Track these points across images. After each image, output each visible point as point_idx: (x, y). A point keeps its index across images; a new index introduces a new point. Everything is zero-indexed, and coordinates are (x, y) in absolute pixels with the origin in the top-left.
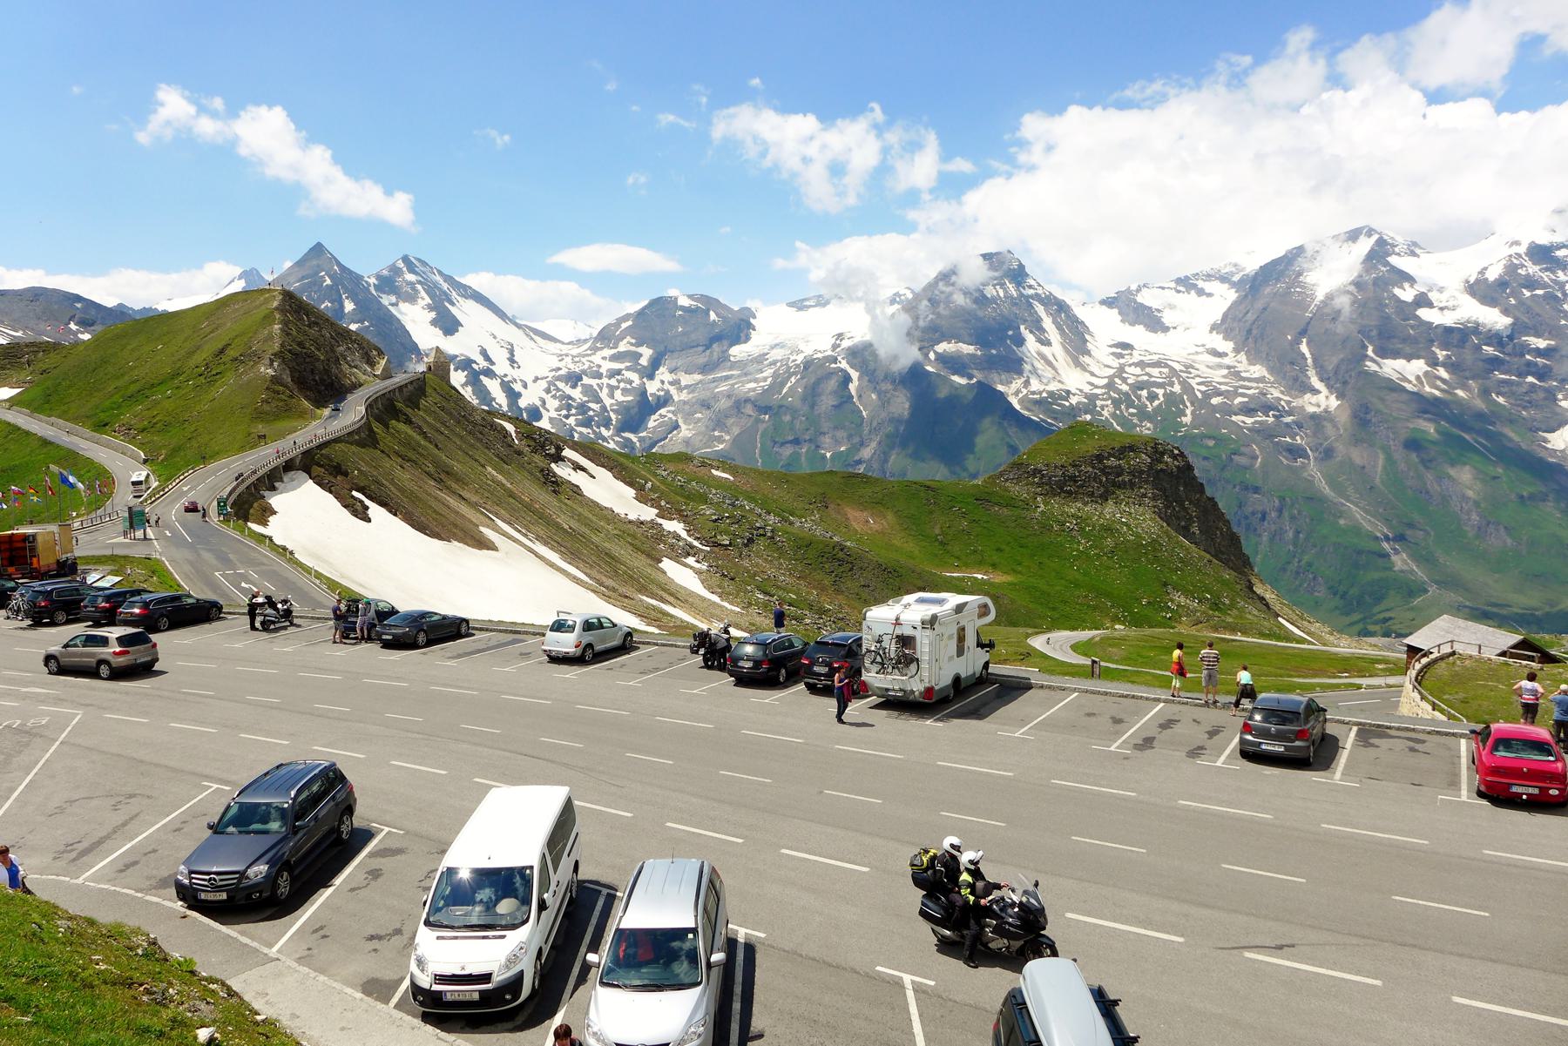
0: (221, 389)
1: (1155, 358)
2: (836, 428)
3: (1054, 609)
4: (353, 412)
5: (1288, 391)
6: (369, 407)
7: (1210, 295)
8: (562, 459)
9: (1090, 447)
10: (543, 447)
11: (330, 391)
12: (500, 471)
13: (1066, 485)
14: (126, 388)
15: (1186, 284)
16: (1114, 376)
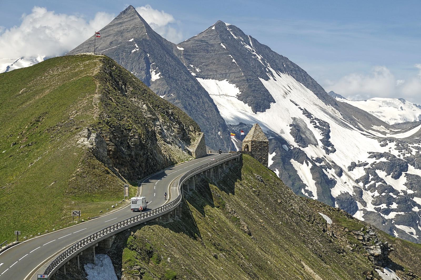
6: (184, 188)
11: (141, 164)
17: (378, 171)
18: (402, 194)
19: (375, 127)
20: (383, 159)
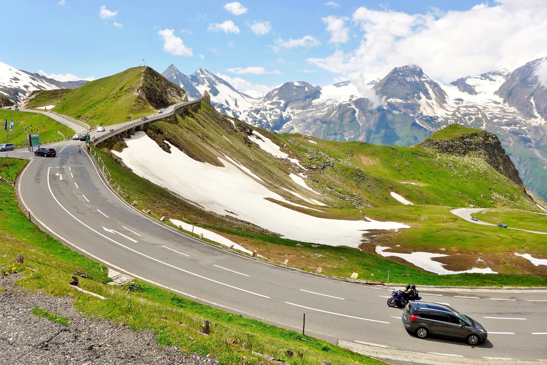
0: (120, 102)
1: (472, 104)
2: (350, 129)
3: (444, 198)
4: (169, 111)
5: (525, 117)
7: (495, 80)
8: (252, 134)
9: (459, 134)
10: (245, 129)
12: (228, 138)
13: (448, 148)
14: (89, 103)
15: (485, 76)
16: (455, 111)
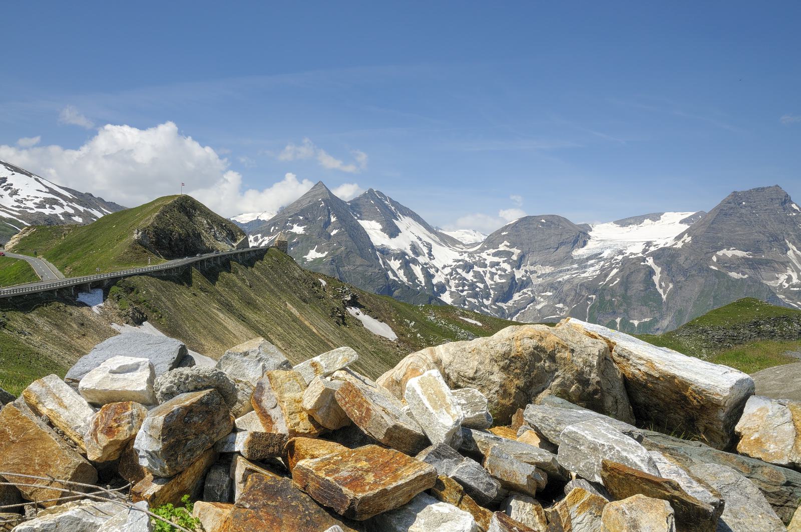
17: (457, 269)
18: (471, 281)
19: (457, 246)
20: (461, 263)
